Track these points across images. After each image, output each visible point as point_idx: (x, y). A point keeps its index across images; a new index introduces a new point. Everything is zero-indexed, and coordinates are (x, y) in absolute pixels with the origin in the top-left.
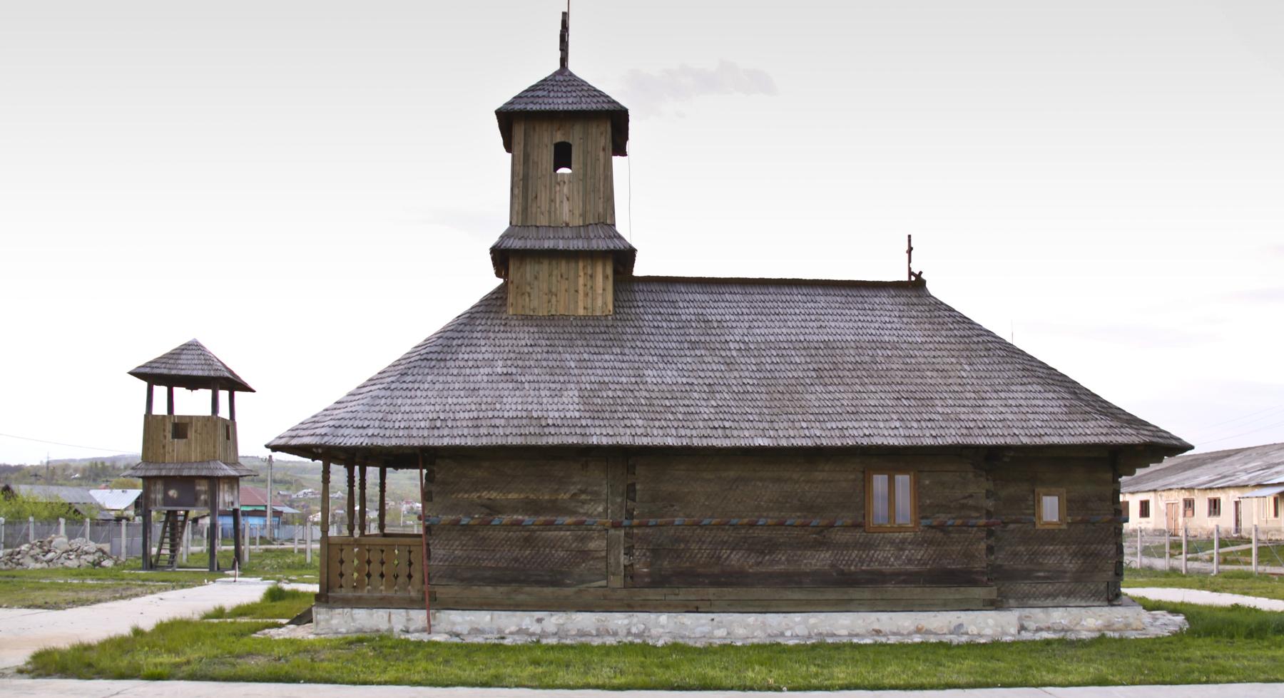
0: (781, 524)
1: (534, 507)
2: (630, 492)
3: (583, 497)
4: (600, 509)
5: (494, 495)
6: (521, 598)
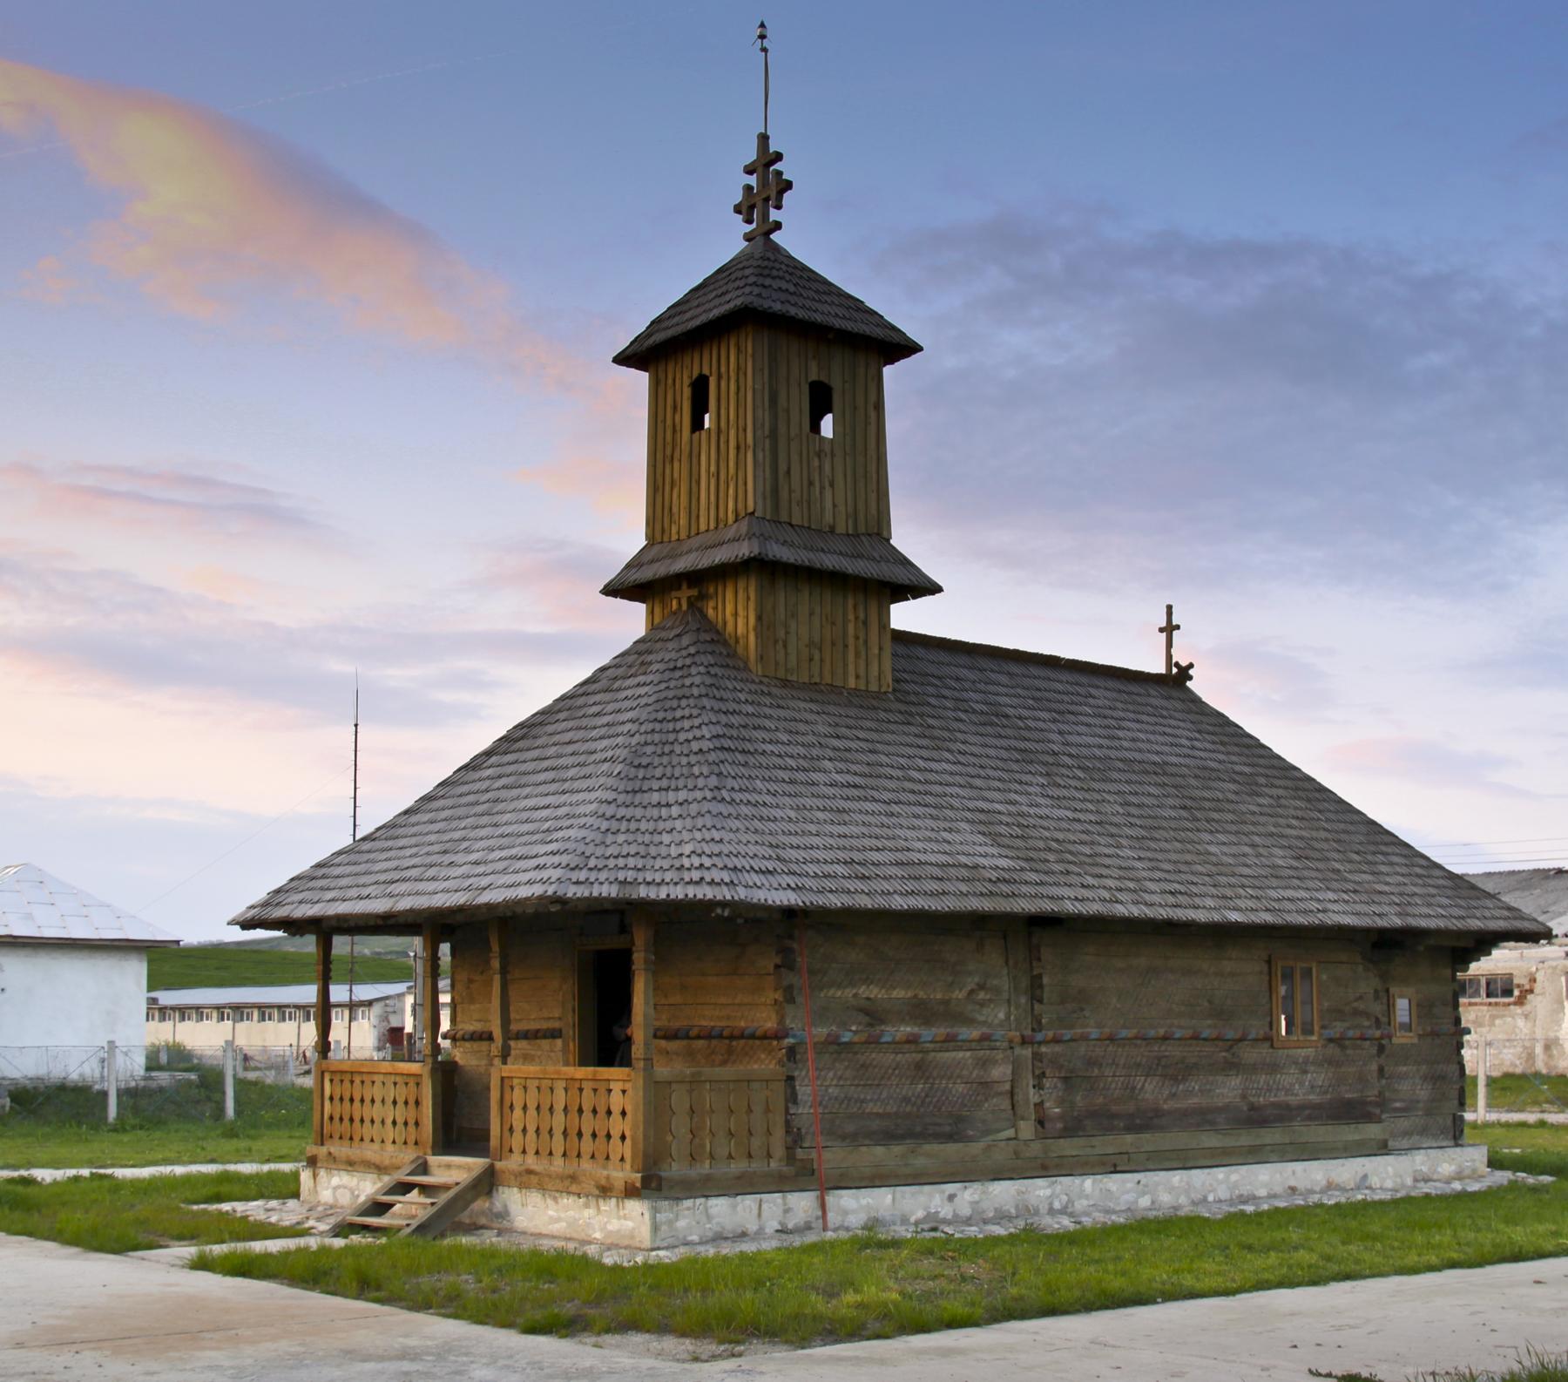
0: (1196, 1037)
1: (921, 1012)
2: (1035, 990)
3: (982, 995)
4: (1001, 1015)
5: (875, 992)
6: (919, 1162)
